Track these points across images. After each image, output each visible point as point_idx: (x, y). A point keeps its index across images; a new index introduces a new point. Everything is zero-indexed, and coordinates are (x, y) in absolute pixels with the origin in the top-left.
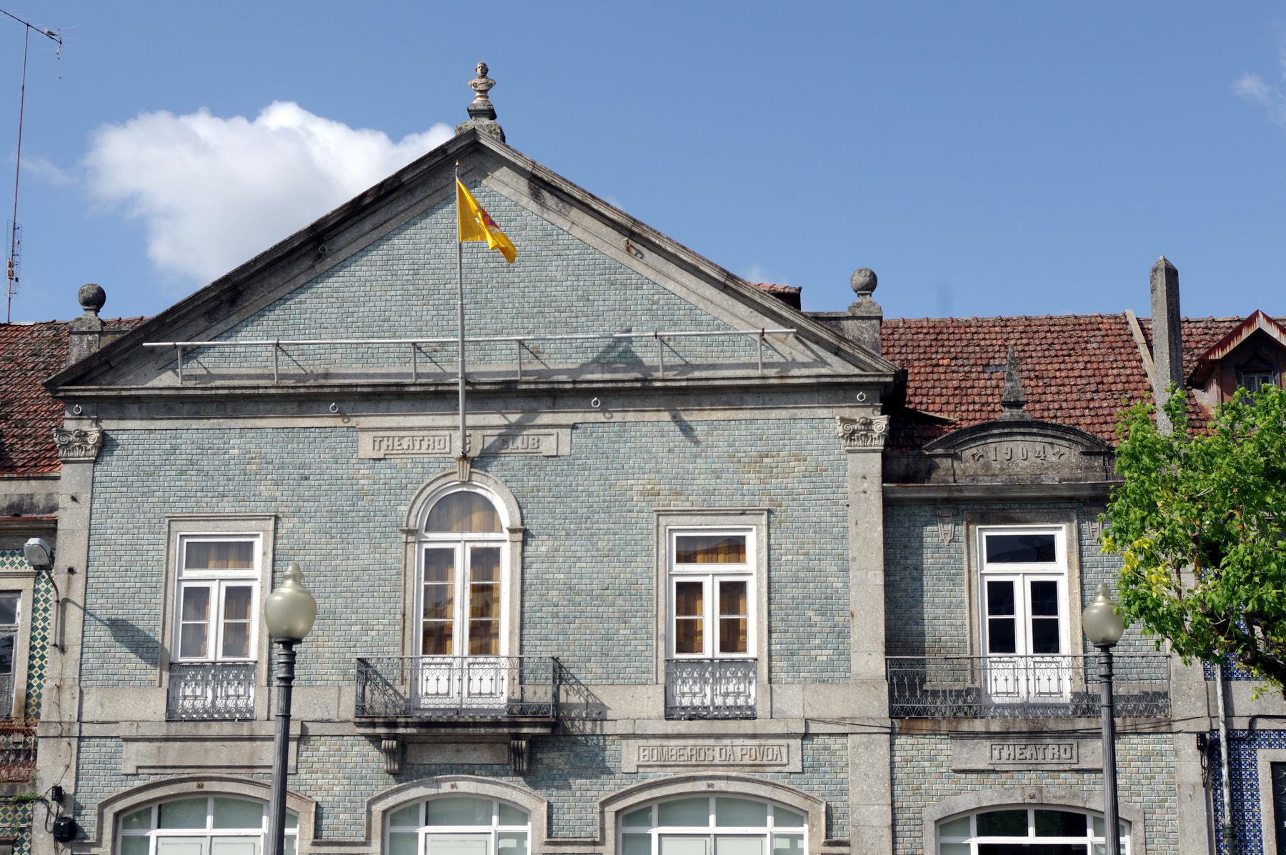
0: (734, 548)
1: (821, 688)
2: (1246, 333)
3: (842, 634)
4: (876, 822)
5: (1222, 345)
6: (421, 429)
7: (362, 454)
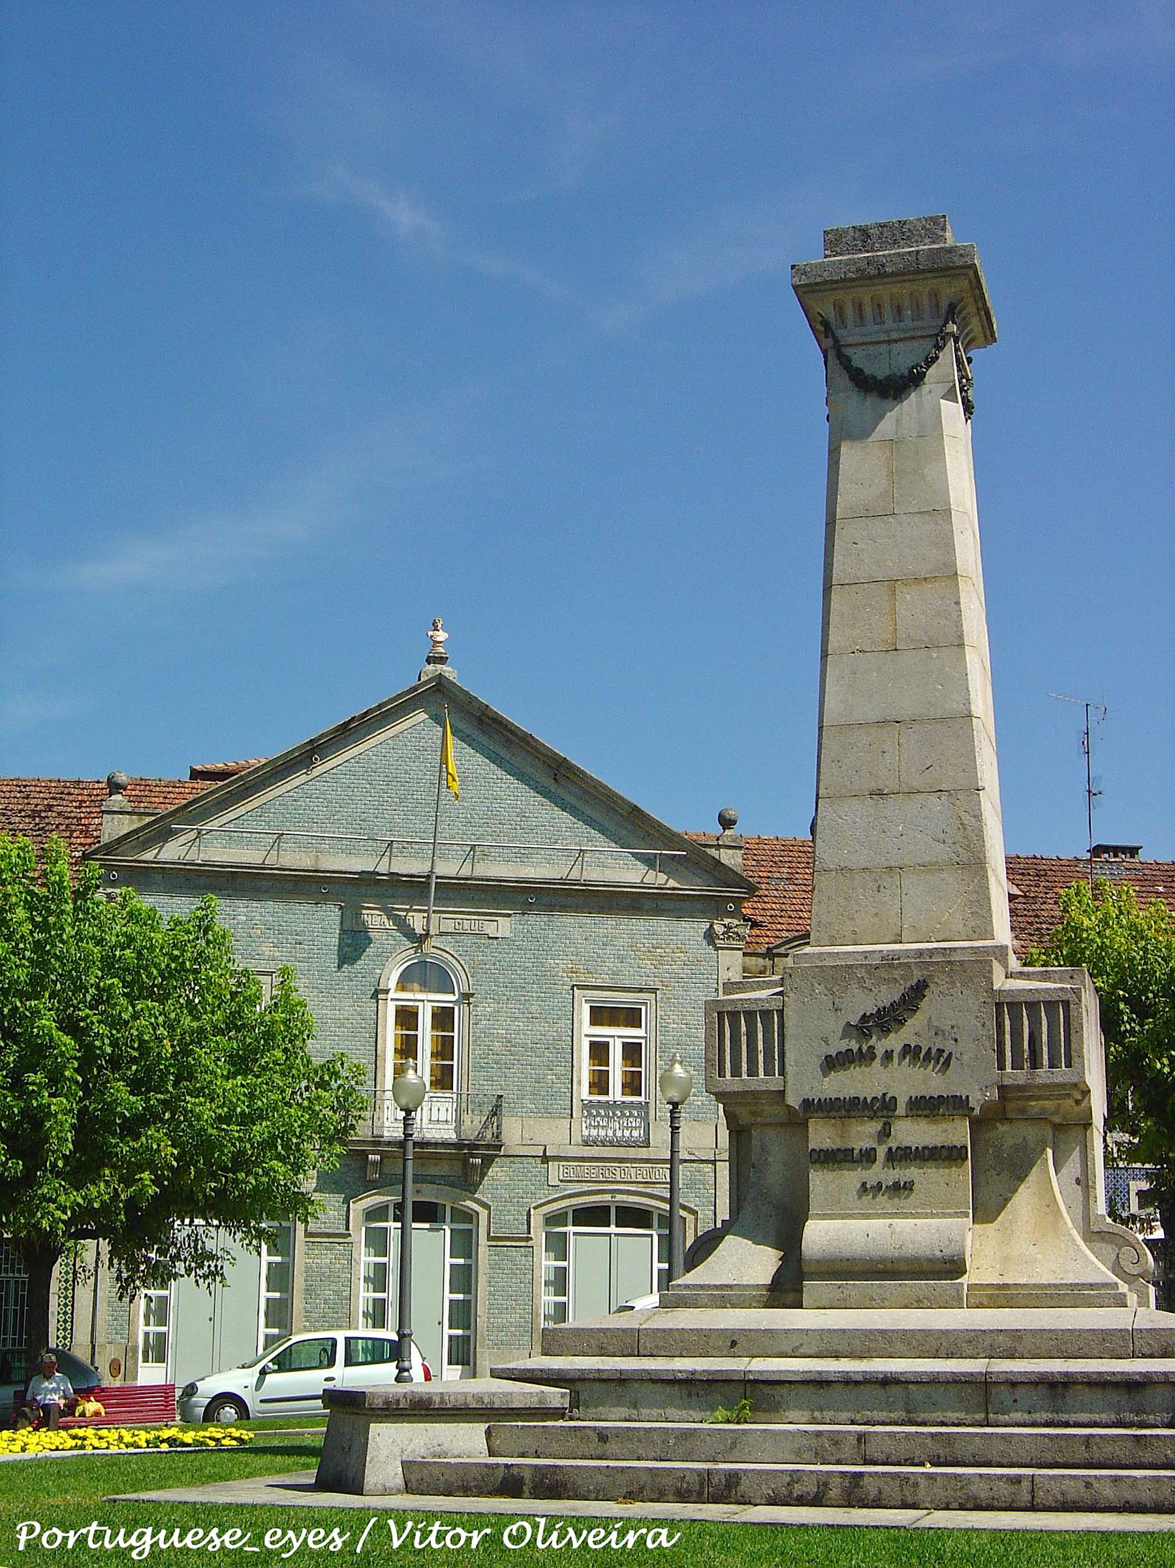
0: (632, 1017)
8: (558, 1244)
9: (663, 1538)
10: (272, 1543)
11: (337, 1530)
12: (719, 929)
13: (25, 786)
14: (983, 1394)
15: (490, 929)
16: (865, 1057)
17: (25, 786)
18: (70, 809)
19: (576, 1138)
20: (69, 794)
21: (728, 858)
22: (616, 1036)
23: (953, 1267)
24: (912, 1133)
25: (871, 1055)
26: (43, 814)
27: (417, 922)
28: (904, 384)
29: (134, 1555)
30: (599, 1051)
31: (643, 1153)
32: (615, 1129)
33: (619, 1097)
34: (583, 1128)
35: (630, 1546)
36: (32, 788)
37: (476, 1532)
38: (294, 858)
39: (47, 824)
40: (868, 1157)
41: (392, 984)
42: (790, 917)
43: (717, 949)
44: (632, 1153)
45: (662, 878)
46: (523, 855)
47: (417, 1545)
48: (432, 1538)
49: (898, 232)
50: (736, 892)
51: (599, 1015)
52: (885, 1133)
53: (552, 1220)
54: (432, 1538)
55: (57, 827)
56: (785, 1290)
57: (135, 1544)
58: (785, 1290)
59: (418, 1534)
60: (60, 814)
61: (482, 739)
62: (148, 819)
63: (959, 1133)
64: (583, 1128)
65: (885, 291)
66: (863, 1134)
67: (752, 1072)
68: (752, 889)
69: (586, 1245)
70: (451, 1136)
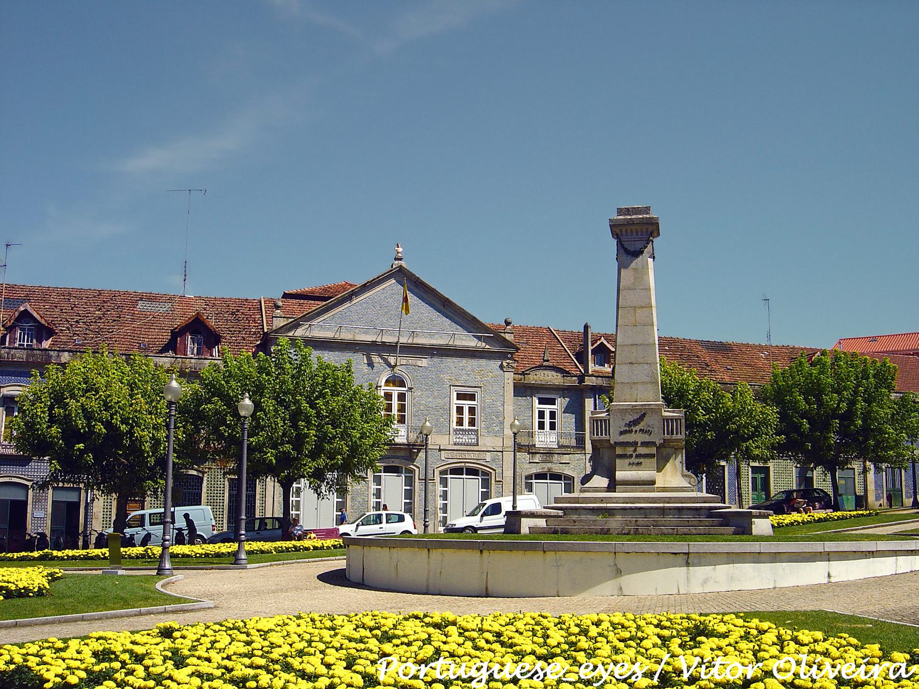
0: (472, 397)
2: (599, 342)
8: (444, 482)
12: (505, 364)
14: (663, 511)
15: (419, 363)
16: (631, 432)
19: (452, 443)
21: (509, 337)
22: (467, 404)
23: (653, 483)
24: (642, 450)
25: (632, 431)
27: (392, 360)
28: (637, 253)
30: (460, 410)
31: (476, 448)
32: (465, 439)
33: (467, 427)
34: (453, 439)
38: (346, 336)
40: (631, 456)
41: (383, 383)
44: (472, 448)
45: (484, 344)
46: (431, 335)
49: (637, 211)
50: (512, 350)
51: (460, 396)
52: (635, 450)
53: (444, 472)
56: (611, 488)
58: (611, 488)
61: (416, 290)
62: (290, 320)
63: (653, 450)
64: (453, 439)
65: (634, 228)
66: (630, 450)
67: (602, 435)
68: (518, 349)
69: (455, 483)
70: (405, 441)
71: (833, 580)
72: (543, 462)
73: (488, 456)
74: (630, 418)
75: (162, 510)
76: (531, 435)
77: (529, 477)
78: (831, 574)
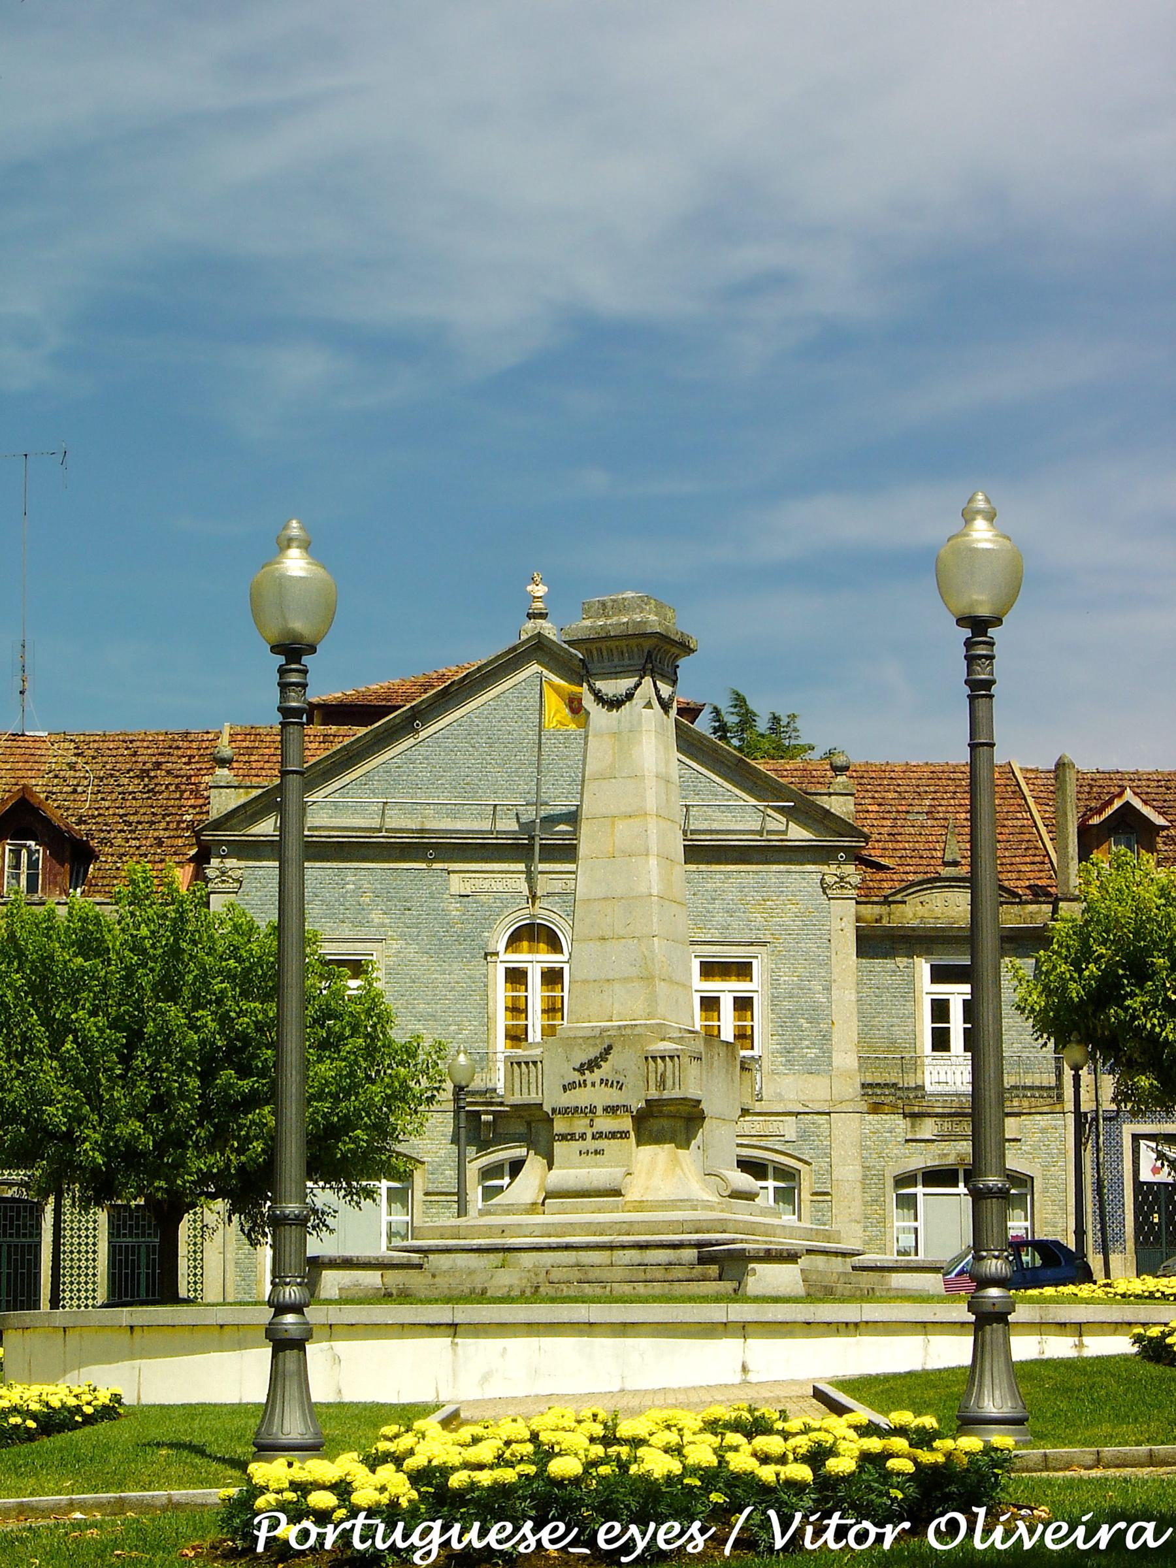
0: (743, 970)
1: (810, 1078)
2: (1117, 804)
3: (826, 1037)
4: (851, 1177)
5: (1099, 812)
6: (499, 872)
7: (453, 891)
9: (1148, 1536)
10: (608, 1542)
11: (697, 1524)
13: (131, 742)
17: (131, 742)
18: (179, 765)
20: (178, 748)
24: (605, 1124)
26: (152, 774)
29: (416, 1558)
35: (1103, 1546)
36: (139, 744)
37: (889, 1527)
39: (156, 785)
40: (583, 1137)
41: (501, 946)
42: (921, 857)
43: (830, 899)
47: (808, 1545)
48: (829, 1535)
51: (709, 970)
54: (829, 1535)
55: (167, 788)
57: (418, 1543)
59: (809, 1530)
60: (169, 772)
71: (752, 1377)
72: (943, 1138)
73: (789, 1129)
74: (582, 1057)
75: (955, 1351)
76: (912, 1064)
77: (904, 1180)
78: (750, 1366)
